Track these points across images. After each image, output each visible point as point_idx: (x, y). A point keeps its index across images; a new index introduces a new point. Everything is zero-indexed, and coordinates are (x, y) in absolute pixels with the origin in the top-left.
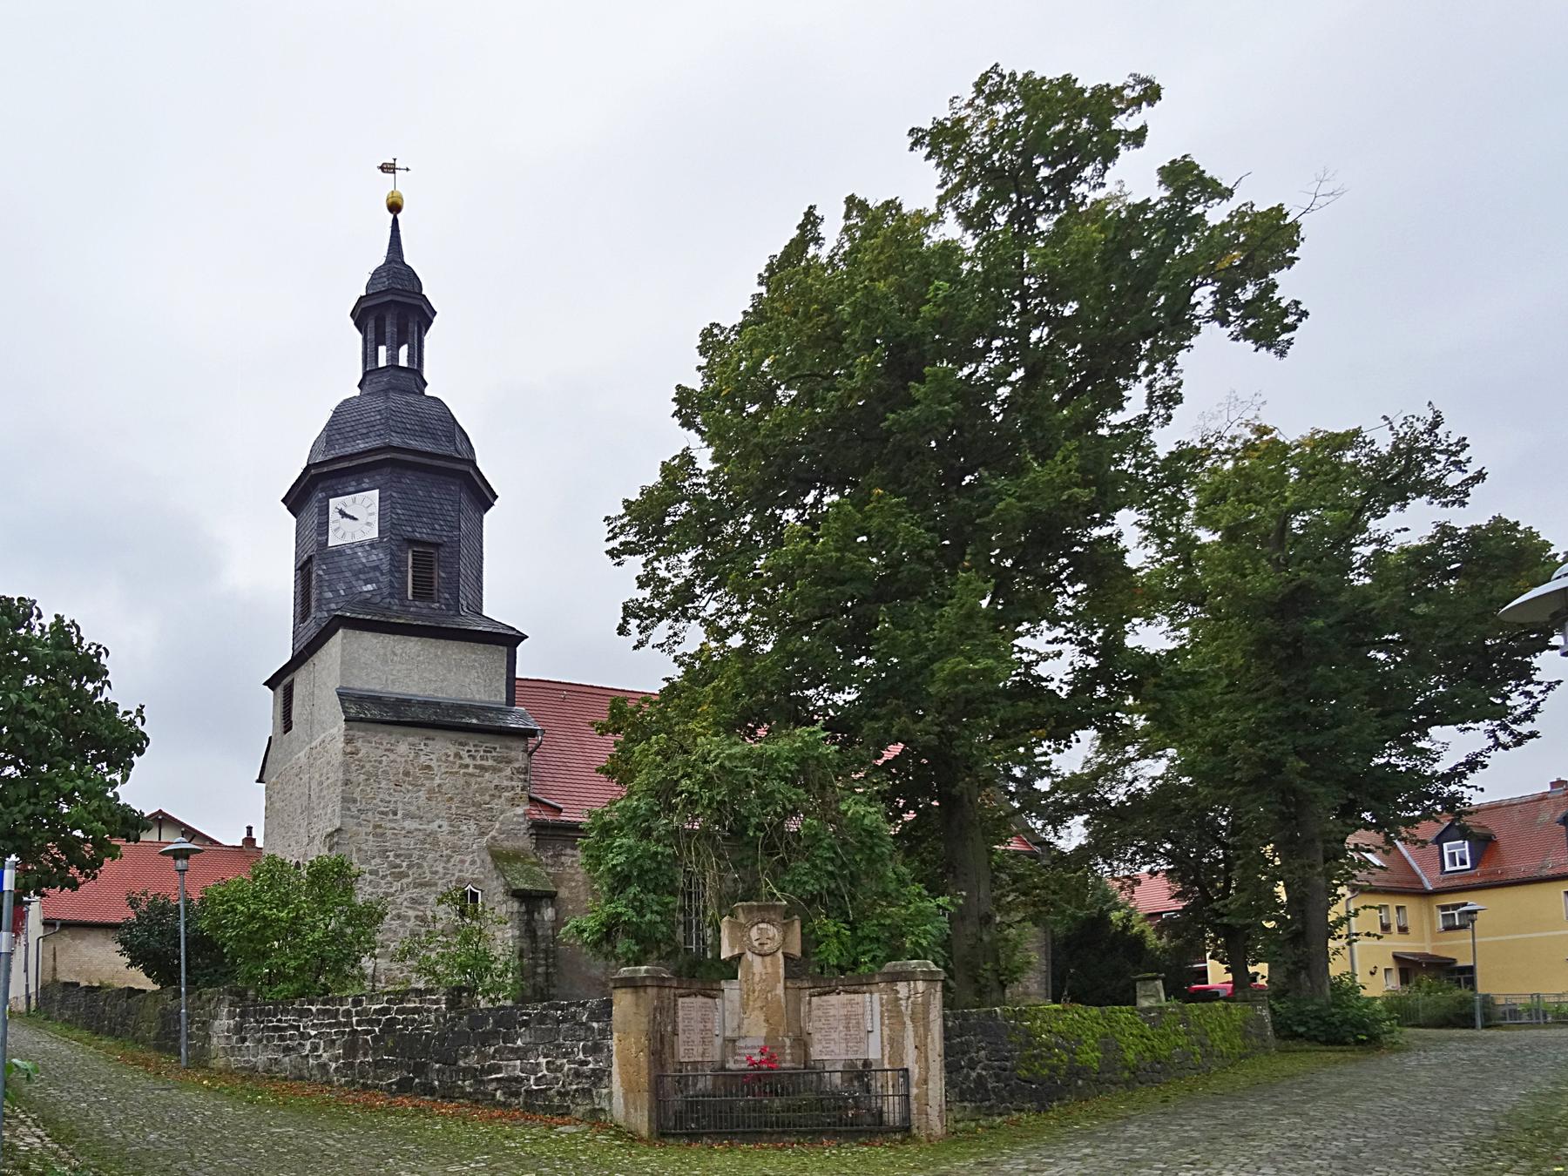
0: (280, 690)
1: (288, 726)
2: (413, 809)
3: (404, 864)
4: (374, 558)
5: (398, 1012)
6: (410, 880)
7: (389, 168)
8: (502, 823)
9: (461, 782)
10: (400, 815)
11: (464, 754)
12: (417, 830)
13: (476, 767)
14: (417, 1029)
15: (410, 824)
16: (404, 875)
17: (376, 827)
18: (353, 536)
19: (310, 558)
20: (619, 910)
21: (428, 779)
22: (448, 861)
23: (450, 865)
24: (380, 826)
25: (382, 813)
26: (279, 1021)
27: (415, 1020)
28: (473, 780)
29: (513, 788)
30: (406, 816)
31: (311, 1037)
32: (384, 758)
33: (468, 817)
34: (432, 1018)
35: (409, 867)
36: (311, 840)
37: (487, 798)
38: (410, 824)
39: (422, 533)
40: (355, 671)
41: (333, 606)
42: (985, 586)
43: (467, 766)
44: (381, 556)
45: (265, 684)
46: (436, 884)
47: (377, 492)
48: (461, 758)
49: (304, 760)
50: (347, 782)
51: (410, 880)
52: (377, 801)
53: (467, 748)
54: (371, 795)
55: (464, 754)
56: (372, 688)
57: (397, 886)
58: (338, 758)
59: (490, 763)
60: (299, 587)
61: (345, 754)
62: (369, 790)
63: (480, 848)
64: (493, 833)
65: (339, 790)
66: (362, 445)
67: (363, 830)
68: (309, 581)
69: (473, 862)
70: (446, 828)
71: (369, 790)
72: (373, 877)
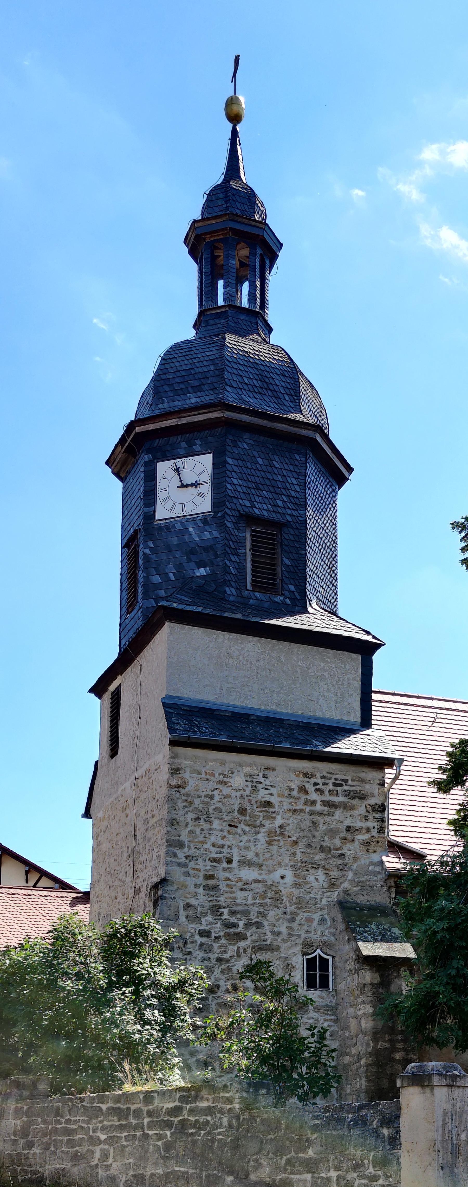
0: (107, 696)
1: (114, 751)
2: (250, 855)
3: (241, 924)
5: (192, 1111)
6: (248, 942)
8: (356, 874)
9: (307, 823)
10: (235, 864)
11: (311, 788)
12: (256, 881)
13: (324, 803)
14: (209, 1133)
15: (248, 874)
16: (240, 937)
17: (208, 877)
18: (184, 509)
19: (136, 532)
20: (437, 988)
21: (267, 818)
22: (293, 920)
23: (295, 925)
24: (212, 877)
25: (215, 860)
26: (68, 1121)
27: (207, 1123)
28: (320, 820)
29: (368, 830)
30: (245, 863)
31: (100, 1142)
32: (216, 793)
33: (315, 866)
34: (225, 1122)
35: (247, 925)
36: (138, 891)
37: (337, 842)
38: (248, 874)
39: (262, 510)
41: (162, 593)
42: (220, 805)
43: (314, 803)
45: (91, 691)
46: (278, 949)
47: (210, 456)
48: (306, 792)
49: (129, 792)
50: (173, 822)
51: (248, 942)
52: (208, 846)
53: (313, 780)
54: (201, 838)
55: (311, 788)
56: (205, 698)
57: (232, 950)
58: (163, 792)
59: (341, 799)
60: (126, 568)
61: (170, 787)
62: (198, 831)
63: (330, 905)
64: (346, 885)
65: (163, 831)
67: (190, 882)
68: (136, 561)
69: (322, 921)
70: (290, 878)
71: (198, 831)
72: (204, 940)
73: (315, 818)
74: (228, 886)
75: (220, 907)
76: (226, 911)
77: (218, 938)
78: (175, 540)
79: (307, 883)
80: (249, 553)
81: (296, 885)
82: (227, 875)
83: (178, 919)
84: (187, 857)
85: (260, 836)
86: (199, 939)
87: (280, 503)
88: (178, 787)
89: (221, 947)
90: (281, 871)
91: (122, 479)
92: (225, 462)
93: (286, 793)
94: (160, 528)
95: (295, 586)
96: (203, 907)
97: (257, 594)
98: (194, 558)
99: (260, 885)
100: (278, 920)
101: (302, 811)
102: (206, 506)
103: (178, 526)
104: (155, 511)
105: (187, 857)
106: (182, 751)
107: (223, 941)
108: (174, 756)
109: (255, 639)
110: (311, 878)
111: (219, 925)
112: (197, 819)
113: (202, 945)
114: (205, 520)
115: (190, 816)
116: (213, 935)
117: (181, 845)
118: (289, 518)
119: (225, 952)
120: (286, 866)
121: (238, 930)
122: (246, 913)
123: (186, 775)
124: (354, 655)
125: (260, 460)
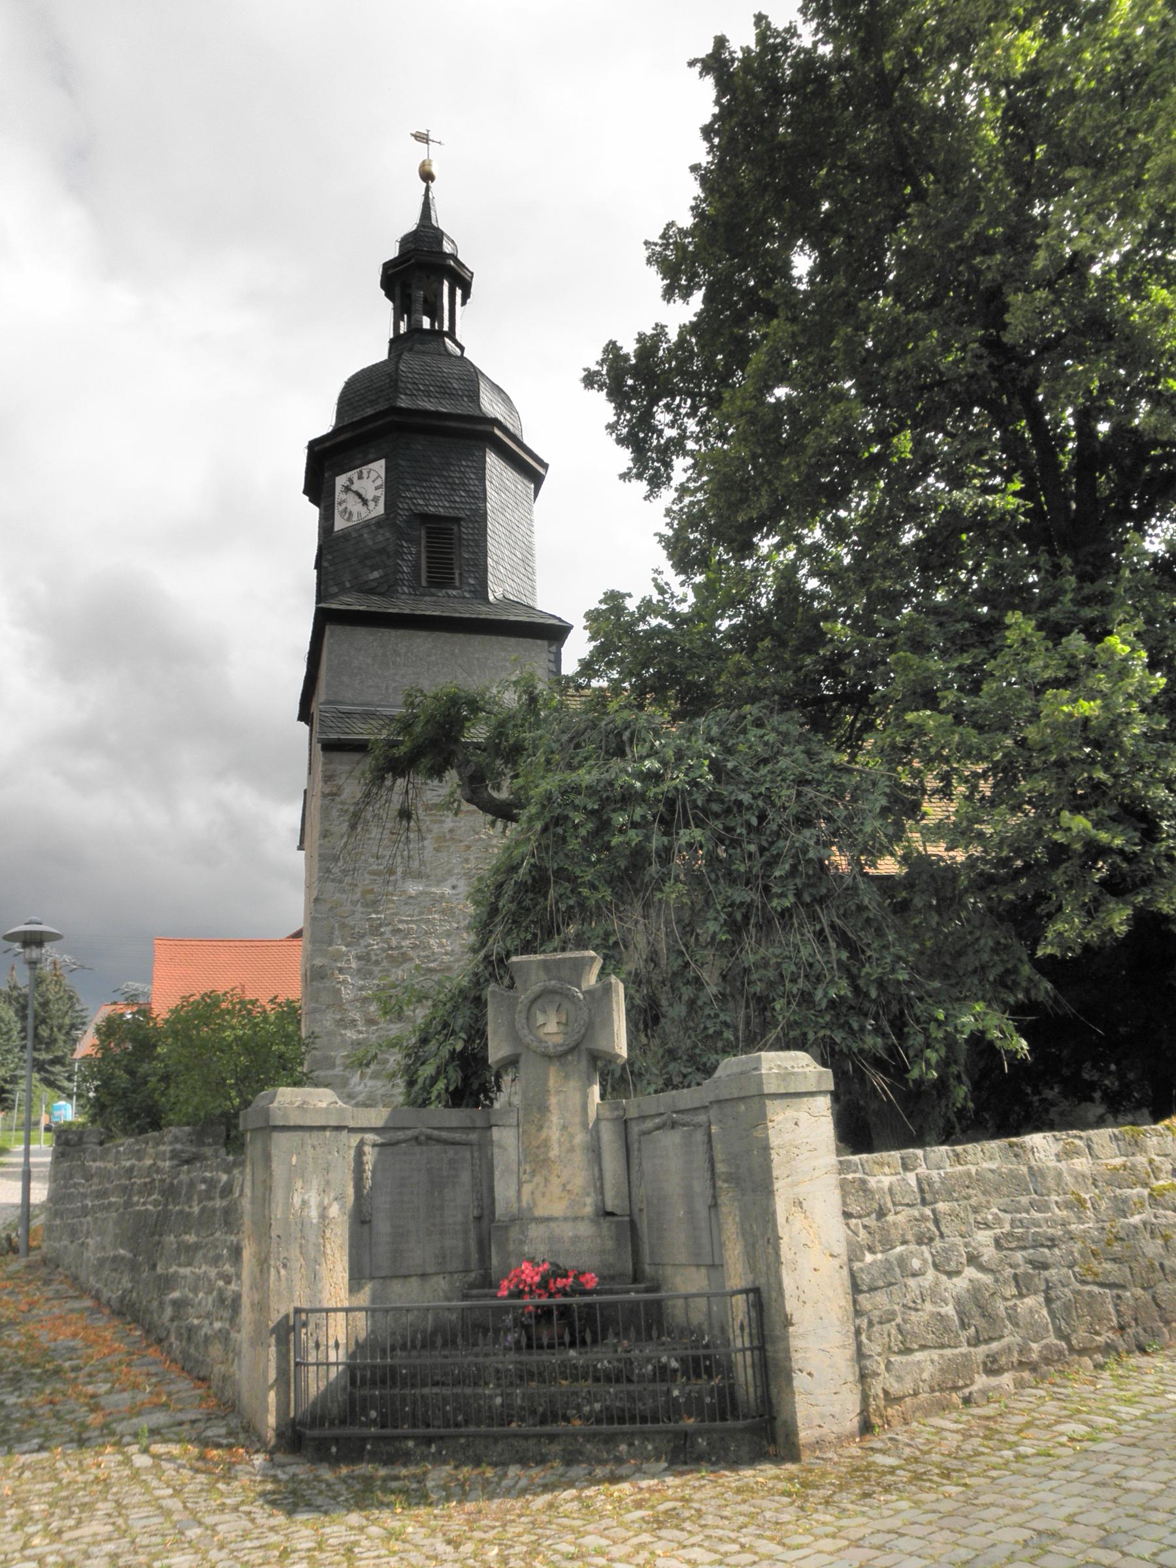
4: (380, 538)
7: (422, 138)
24: (371, 891)
40: (346, 679)
44: (388, 535)
66: (370, 411)
85: (426, 843)
90: (453, 881)
98: (368, 563)
103: (354, 535)
106: (336, 756)
107: (385, 964)
109: (424, 633)
114: (379, 523)
124: (539, 642)
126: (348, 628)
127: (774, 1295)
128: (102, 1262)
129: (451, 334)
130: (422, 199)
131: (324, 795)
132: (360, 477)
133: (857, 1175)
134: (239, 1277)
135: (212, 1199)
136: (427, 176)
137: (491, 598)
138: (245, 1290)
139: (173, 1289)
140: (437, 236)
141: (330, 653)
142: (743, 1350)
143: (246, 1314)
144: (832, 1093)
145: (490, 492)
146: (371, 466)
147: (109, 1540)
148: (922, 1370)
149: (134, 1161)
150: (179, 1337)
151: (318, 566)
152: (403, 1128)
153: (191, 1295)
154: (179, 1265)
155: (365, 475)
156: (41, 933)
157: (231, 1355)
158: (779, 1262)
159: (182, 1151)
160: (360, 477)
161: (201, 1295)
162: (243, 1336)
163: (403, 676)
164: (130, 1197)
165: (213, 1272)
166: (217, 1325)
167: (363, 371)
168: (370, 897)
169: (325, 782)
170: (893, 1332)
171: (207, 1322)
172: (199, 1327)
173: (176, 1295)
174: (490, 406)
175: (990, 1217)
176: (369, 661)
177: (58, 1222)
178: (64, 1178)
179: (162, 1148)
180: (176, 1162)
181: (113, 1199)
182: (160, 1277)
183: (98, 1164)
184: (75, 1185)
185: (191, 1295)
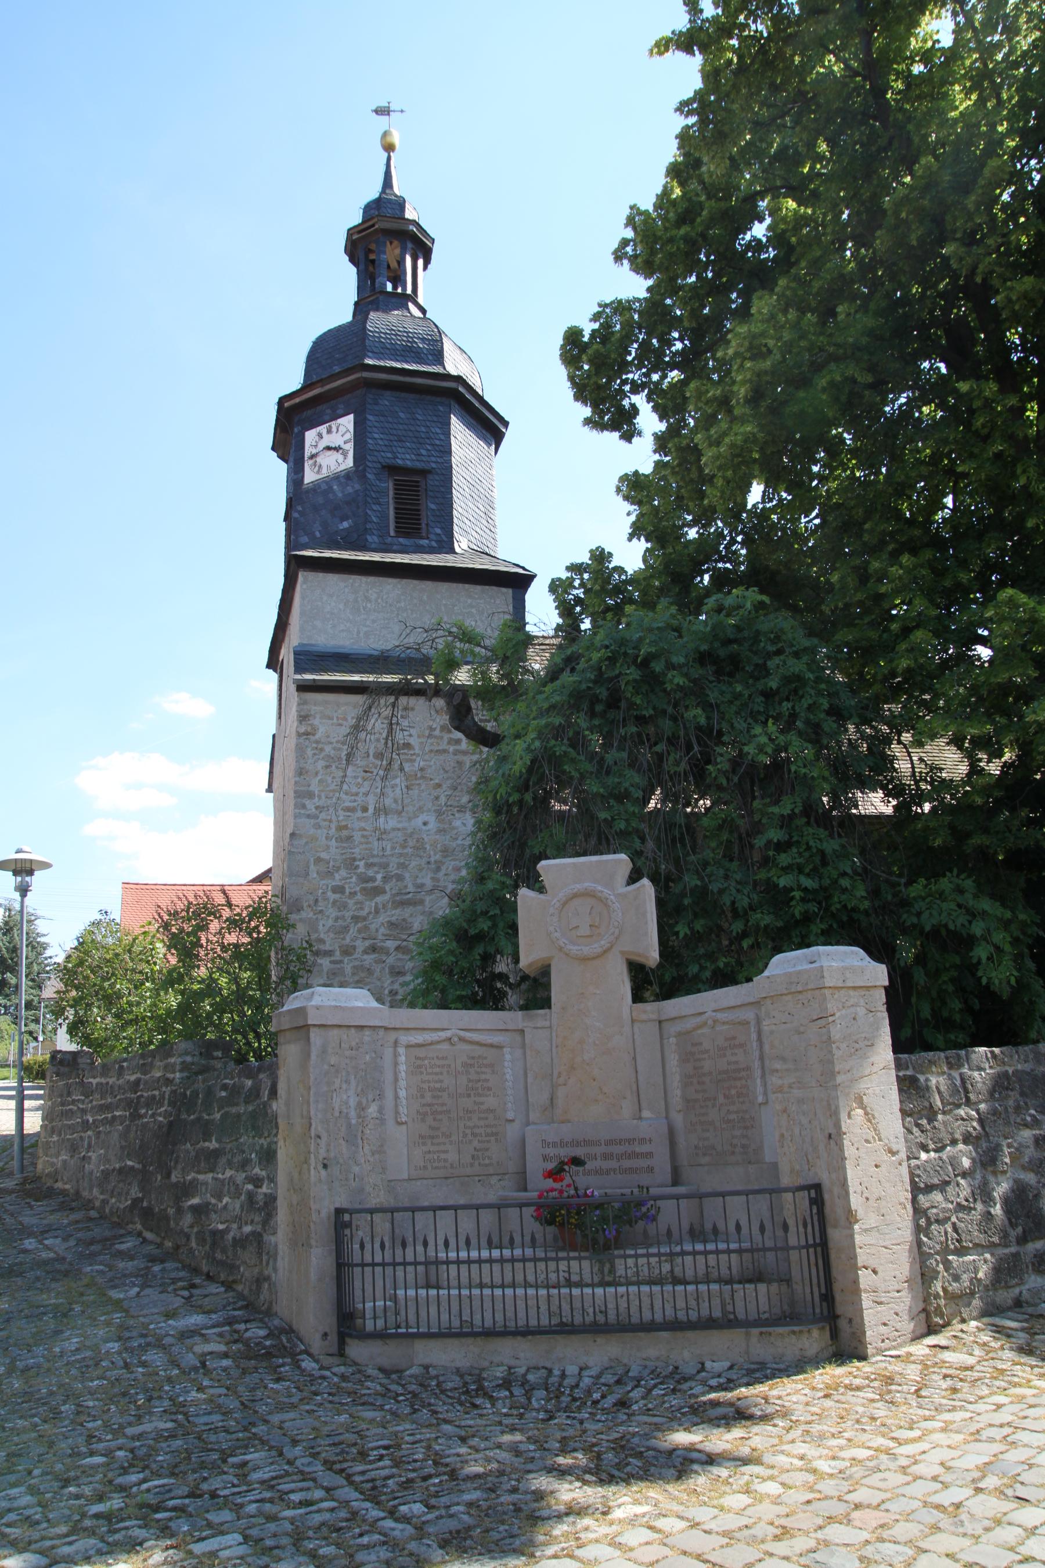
3: (379, 877)
12: (394, 829)
16: (378, 891)
17: (340, 828)
24: (346, 827)
25: (348, 809)
35: (386, 879)
46: (421, 902)
56: (341, 643)
57: (369, 905)
62: (329, 780)
70: (433, 825)
71: (329, 780)
72: (337, 896)
73: (460, 757)
74: (363, 836)
75: (354, 860)
76: (362, 863)
77: (353, 894)
78: (320, 500)
79: (454, 828)
80: (391, 501)
81: (440, 831)
82: (363, 824)
83: (308, 874)
84: (317, 808)
86: (332, 896)
87: (424, 452)
88: (307, 734)
89: (356, 903)
91: (286, 461)
92: (366, 419)
93: (427, 733)
94: (308, 491)
95: (442, 528)
96: (335, 860)
97: (401, 540)
99: (400, 834)
100: (421, 870)
101: (445, 751)
102: (350, 462)
103: (324, 487)
104: (303, 477)
105: (317, 808)
107: (359, 897)
108: (302, 703)
110: (457, 823)
111: (354, 879)
112: (327, 767)
113: (335, 902)
114: (346, 477)
115: (321, 764)
116: (347, 891)
117: (310, 795)
118: (434, 465)
119: (362, 909)
120: (429, 810)
121: (376, 884)
122: (385, 866)
123: (316, 722)
124: (504, 590)
125: (402, 415)
126: (321, 575)
127: (836, 1190)
128: (106, 1174)
129: (413, 298)
130: (384, 168)
131: (299, 735)
132: (329, 431)
133: (908, 1073)
134: (272, 1179)
135: (237, 1104)
136: (389, 148)
137: (457, 549)
138: (281, 1194)
139: (193, 1197)
140: (400, 204)
141: (303, 598)
142: (799, 1248)
143: (282, 1216)
144: (885, 988)
145: (454, 447)
146: (340, 421)
147: (173, 1436)
148: (976, 1271)
149: (139, 1075)
150: (202, 1241)
151: (287, 518)
152: (443, 1030)
153: (213, 1201)
154: (199, 1172)
155: (334, 429)
156: (31, 861)
157: (265, 1258)
158: (844, 1159)
159: (193, 1064)
160: (329, 431)
161: (226, 1200)
162: (280, 1238)
163: (374, 621)
164: (136, 1110)
165: (240, 1177)
166: (247, 1229)
167: (325, 334)
168: (345, 833)
169: (300, 722)
170: (950, 1230)
171: (235, 1226)
172: (227, 1231)
173: (195, 1201)
174: (454, 364)
175: (1029, 1119)
176: (341, 606)
177: (55, 1138)
178: (61, 1096)
179: (172, 1060)
180: (185, 1074)
181: (117, 1114)
182: (176, 1185)
183: (98, 1080)
184: (74, 1102)
185: (213, 1201)
